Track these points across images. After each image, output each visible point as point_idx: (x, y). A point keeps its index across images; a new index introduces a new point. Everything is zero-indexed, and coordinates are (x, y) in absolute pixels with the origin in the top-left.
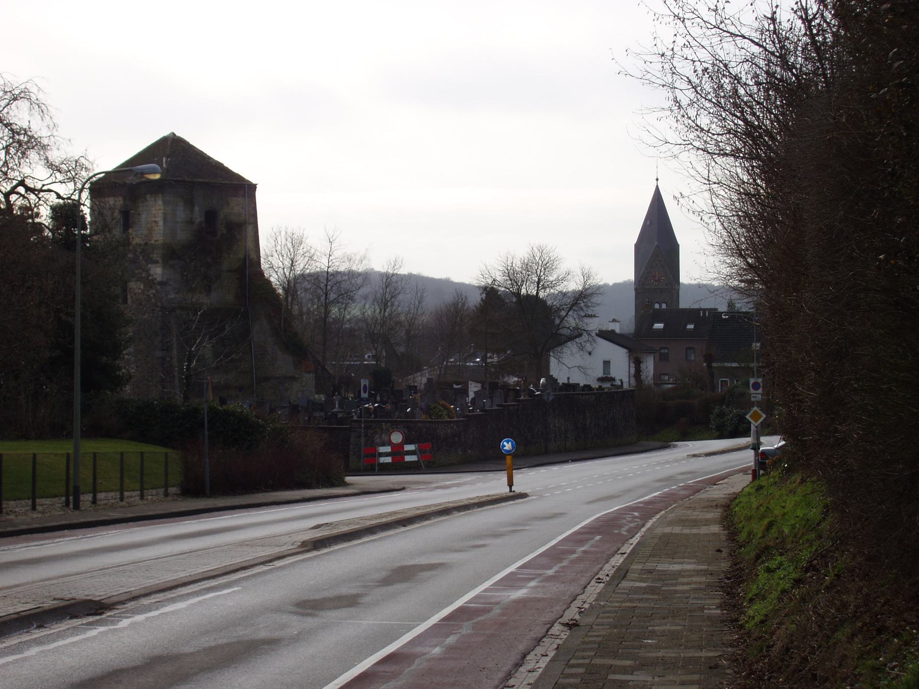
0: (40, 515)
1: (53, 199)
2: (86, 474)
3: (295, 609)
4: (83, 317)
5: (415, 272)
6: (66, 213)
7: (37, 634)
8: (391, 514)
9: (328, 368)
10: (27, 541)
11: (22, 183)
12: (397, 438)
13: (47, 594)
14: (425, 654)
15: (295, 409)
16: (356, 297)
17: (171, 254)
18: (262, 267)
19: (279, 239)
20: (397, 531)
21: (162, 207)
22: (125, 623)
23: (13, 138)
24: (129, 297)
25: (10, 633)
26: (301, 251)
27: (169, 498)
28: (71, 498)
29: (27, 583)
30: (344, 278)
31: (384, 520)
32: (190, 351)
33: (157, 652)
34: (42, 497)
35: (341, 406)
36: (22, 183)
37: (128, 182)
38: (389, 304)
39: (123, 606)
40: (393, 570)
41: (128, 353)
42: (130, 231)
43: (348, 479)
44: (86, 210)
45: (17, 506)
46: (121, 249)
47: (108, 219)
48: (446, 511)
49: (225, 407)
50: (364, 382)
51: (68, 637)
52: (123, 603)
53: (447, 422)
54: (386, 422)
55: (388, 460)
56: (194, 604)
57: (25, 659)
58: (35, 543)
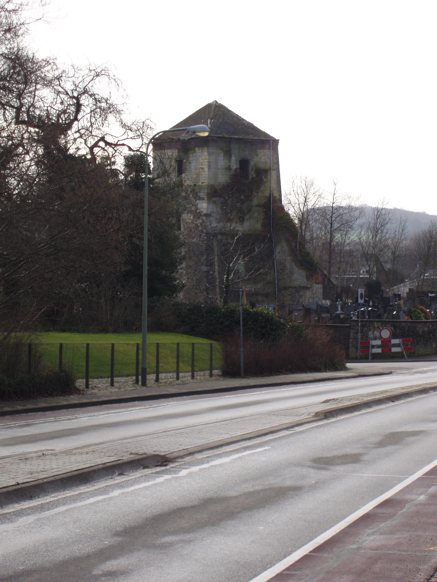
0: (117, 390)
1: (126, 152)
2: (151, 359)
3: (312, 464)
4: (149, 241)
5: (399, 207)
6: (136, 162)
7: (119, 479)
8: (382, 392)
9: (333, 280)
10: (108, 409)
11: (102, 139)
12: (386, 334)
13: (125, 450)
14: (414, 500)
15: (308, 311)
16: (354, 226)
17: (214, 193)
18: (283, 203)
19: (295, 182)
20: (388, 405)
21: (207, 157)
22: (184, 473)
23: (96, 105)
24: (182, 225)
25: (98, 479)
26: (312, 191)
27: (213, 378)
28: (140, 377)
29: (110, 441)
30: (347, 211)
31: (377, 397)
32: (229, 267)
33: (210, 495)
34: (118, 376)
35: (342, 309)
36: (102, 139)
37: (182, 138)
38: (380, 231)
39: (182, 460)
40: (386, 436)
41: (182, 268)
42: (183, 175)
43: (348, 365)
44: (150, 159)
45: (99, 383)
46: (176, 189)
47: (167, 166)
48: (424, 391)
49: (255, 309)
50: (361, 291)
51: (142, 482)
52: (182, 457)
53: (424, 322)
54: (378, 322)
55: (379, 350)
56: (236, 459)
57: (111, 499)
58: (113, 411)
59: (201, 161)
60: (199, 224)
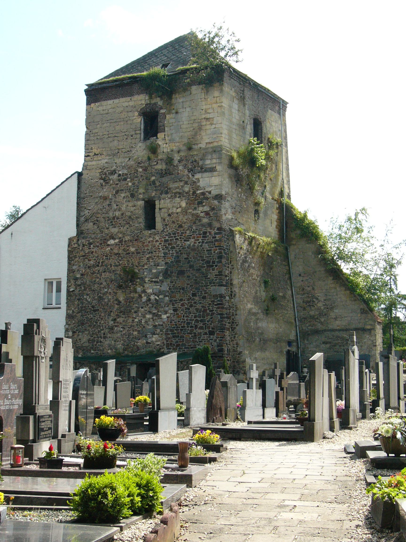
59: (204, 107)
60: (202, 215)
